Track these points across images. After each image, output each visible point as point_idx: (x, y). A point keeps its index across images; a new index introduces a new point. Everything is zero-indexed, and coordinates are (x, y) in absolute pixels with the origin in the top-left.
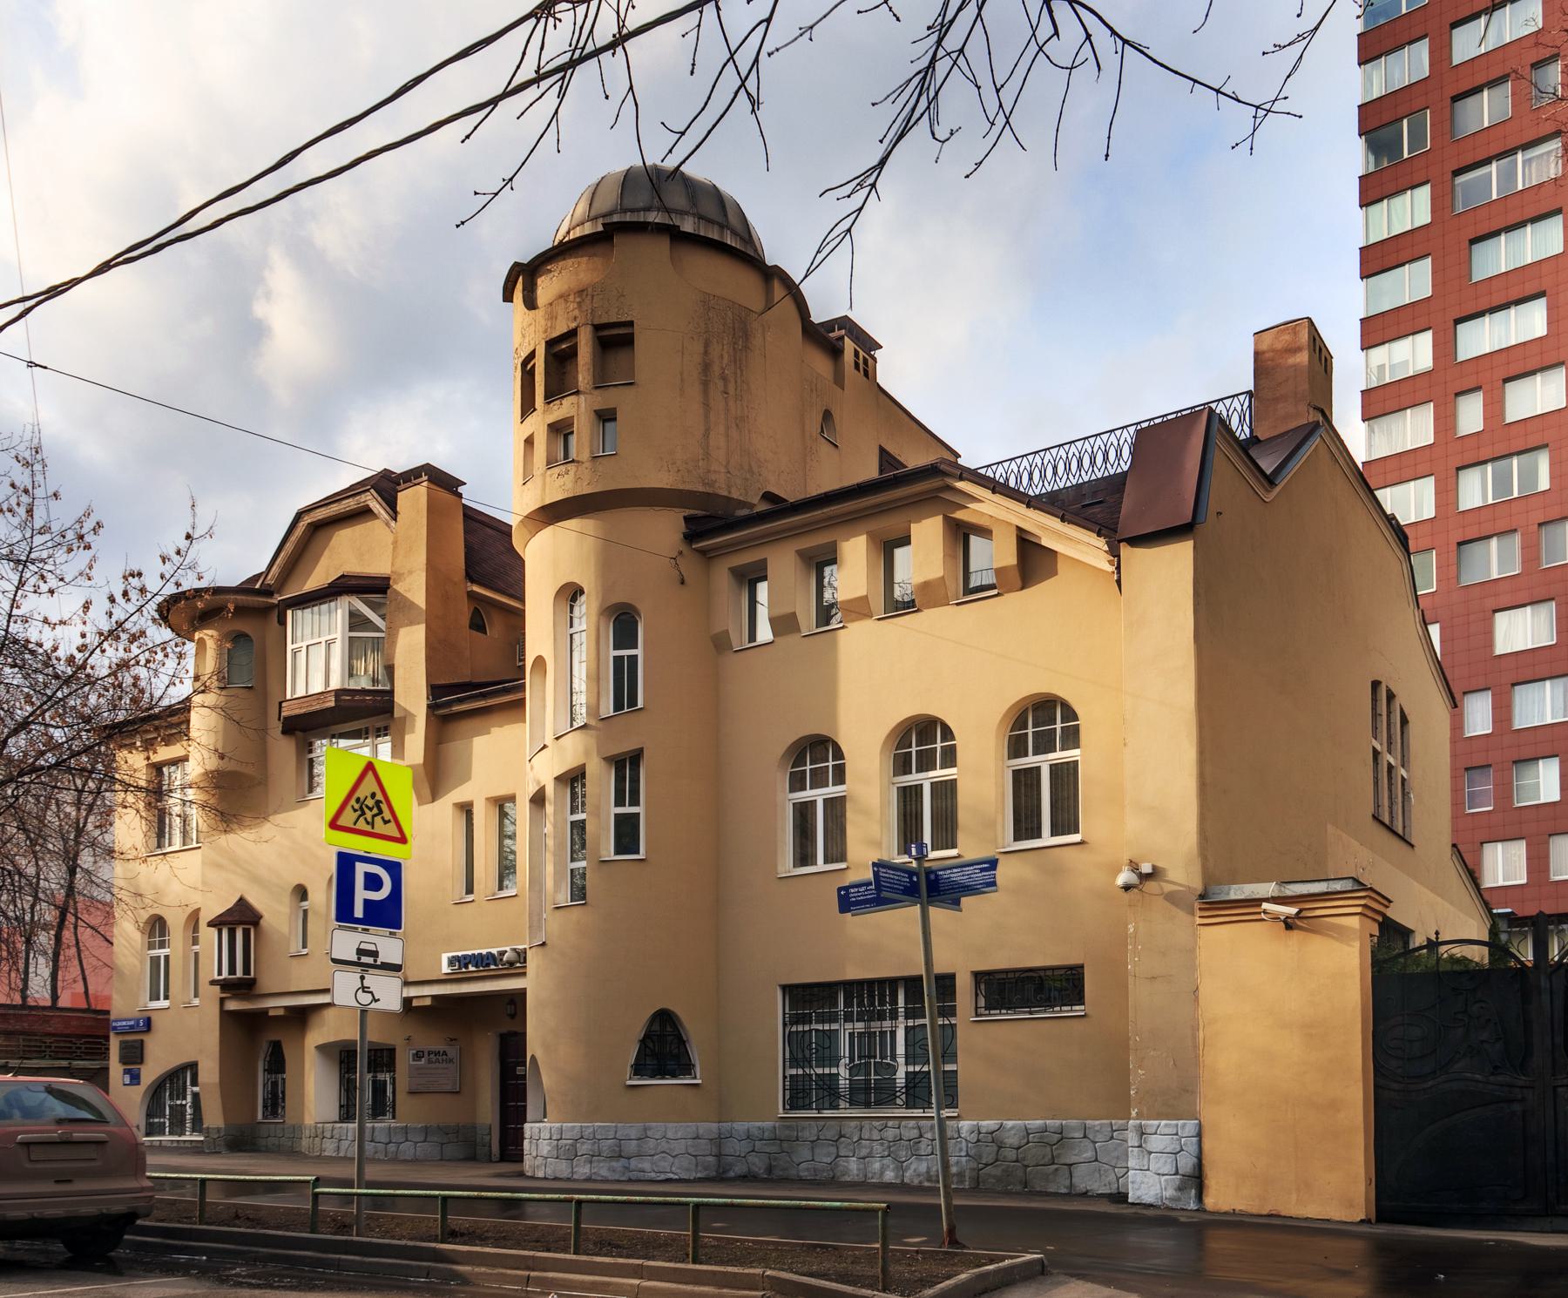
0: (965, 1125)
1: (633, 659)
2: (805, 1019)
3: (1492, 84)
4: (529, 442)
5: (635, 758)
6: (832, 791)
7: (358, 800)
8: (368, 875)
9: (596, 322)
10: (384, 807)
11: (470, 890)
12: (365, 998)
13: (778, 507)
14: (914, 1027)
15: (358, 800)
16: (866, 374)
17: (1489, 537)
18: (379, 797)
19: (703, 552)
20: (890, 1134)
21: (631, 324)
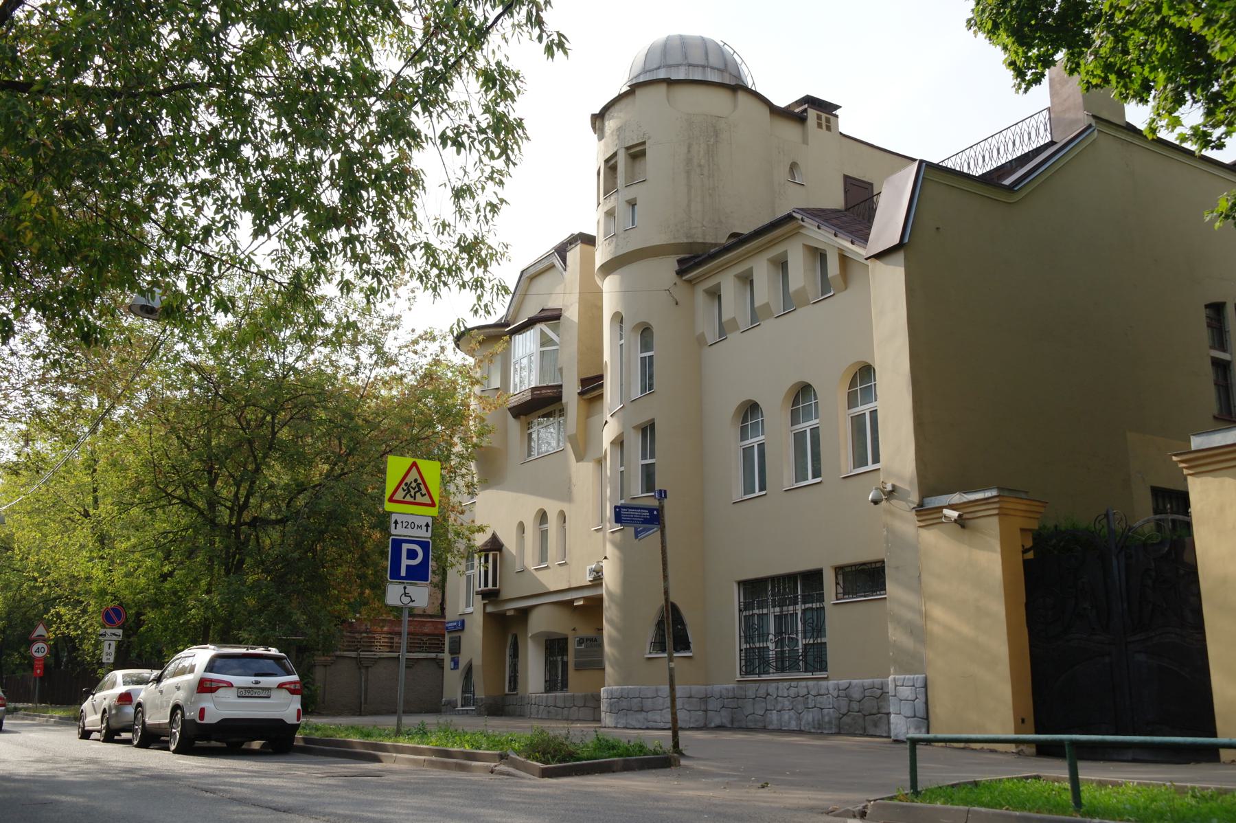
0: (831, 683)
2: (1164, 511)
12: (406, 600)
13: (739, 240)
18: (420, 481)
19: (689, 281)
20: (793, 692)
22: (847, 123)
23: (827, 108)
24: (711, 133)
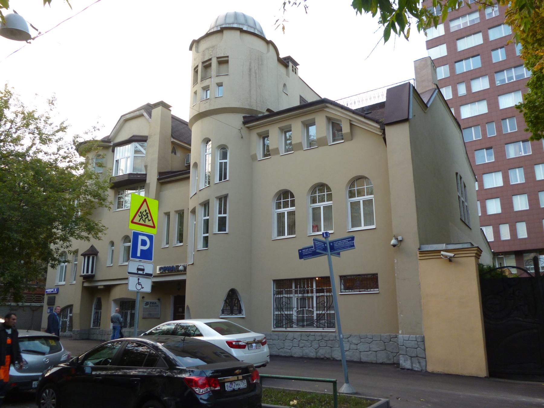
1: (226, 163)
3: (501, 48)
4: (195, 93)
5: (226, 197)
6: (290, 209)
7: (141, 212)
8: (142, 240)
9: (218, 56)
10: (149, 215)
11: (37, 30)
13: (271, 114)
14: (319, 296)
15: (141, 212)
16: (296, 73)
17: (471, 127)
18: (148, 211)
19: (248, 128)
21: (228, 57)
22: (302, 72)
23: (295, 64)
24: (260, 60)
